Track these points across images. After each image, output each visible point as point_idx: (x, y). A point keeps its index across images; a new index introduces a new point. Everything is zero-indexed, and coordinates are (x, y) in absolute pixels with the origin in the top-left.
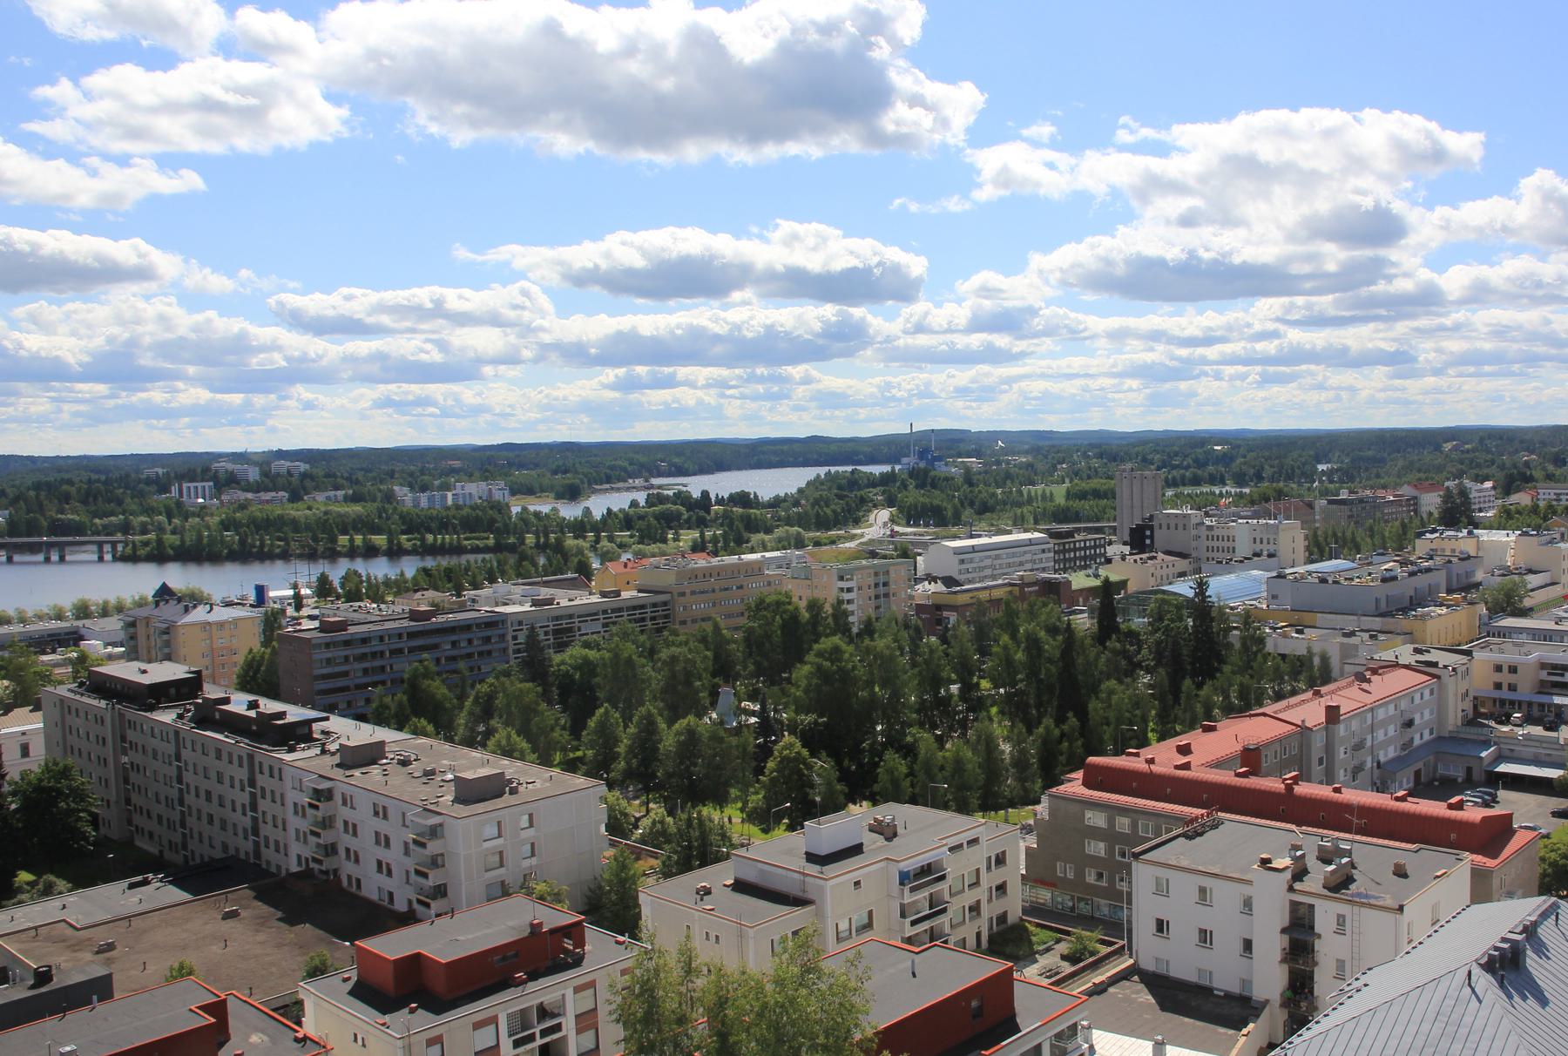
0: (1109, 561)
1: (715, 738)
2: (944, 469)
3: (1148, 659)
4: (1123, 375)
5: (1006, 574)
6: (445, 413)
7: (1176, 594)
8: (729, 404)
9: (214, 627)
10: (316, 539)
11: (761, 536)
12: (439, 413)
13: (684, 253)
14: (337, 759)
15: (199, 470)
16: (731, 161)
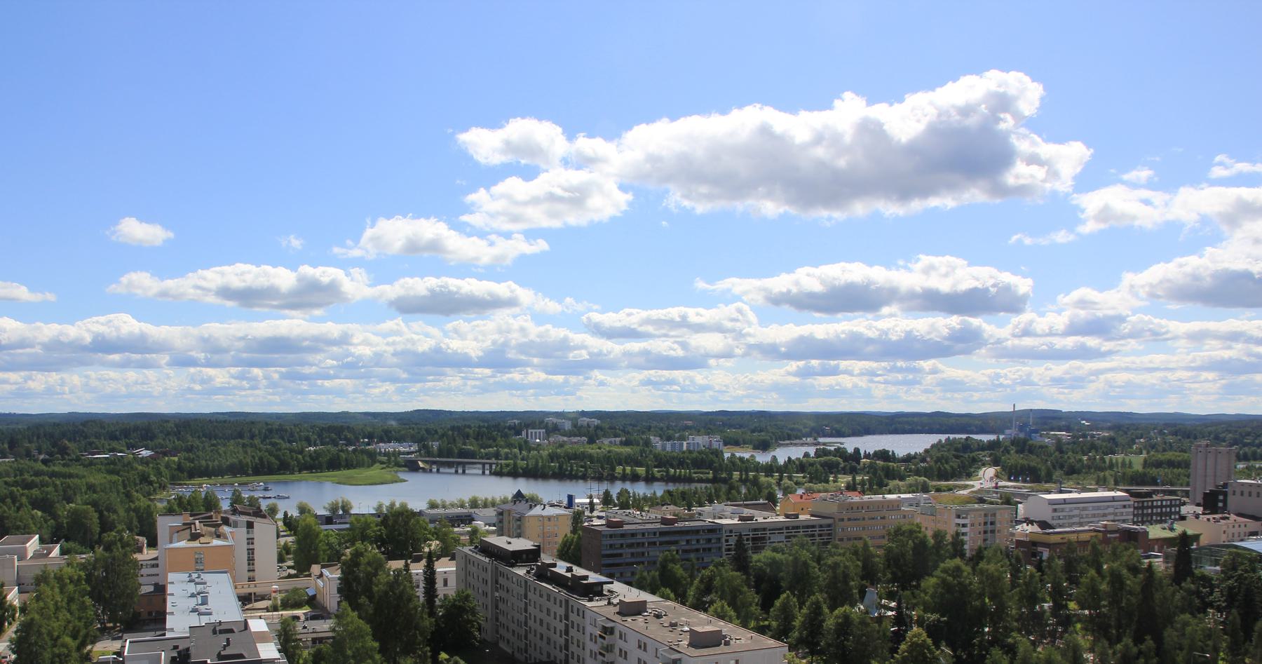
0: (1183, 518)
1: (863, 623)
2: (1039, 439)
3: (1219, 601)
4: (1201, 368)
5: (1091, 522)
6: (684, 390)
7: (1249, 550)
8: (876, 387)
9: (546, 519)
10: (603, 468)
11: (897, 482)
12: (680, 389)
13: (849, 281)
14: (617, 609)
15: (537, 422)
16: (887, 213)
